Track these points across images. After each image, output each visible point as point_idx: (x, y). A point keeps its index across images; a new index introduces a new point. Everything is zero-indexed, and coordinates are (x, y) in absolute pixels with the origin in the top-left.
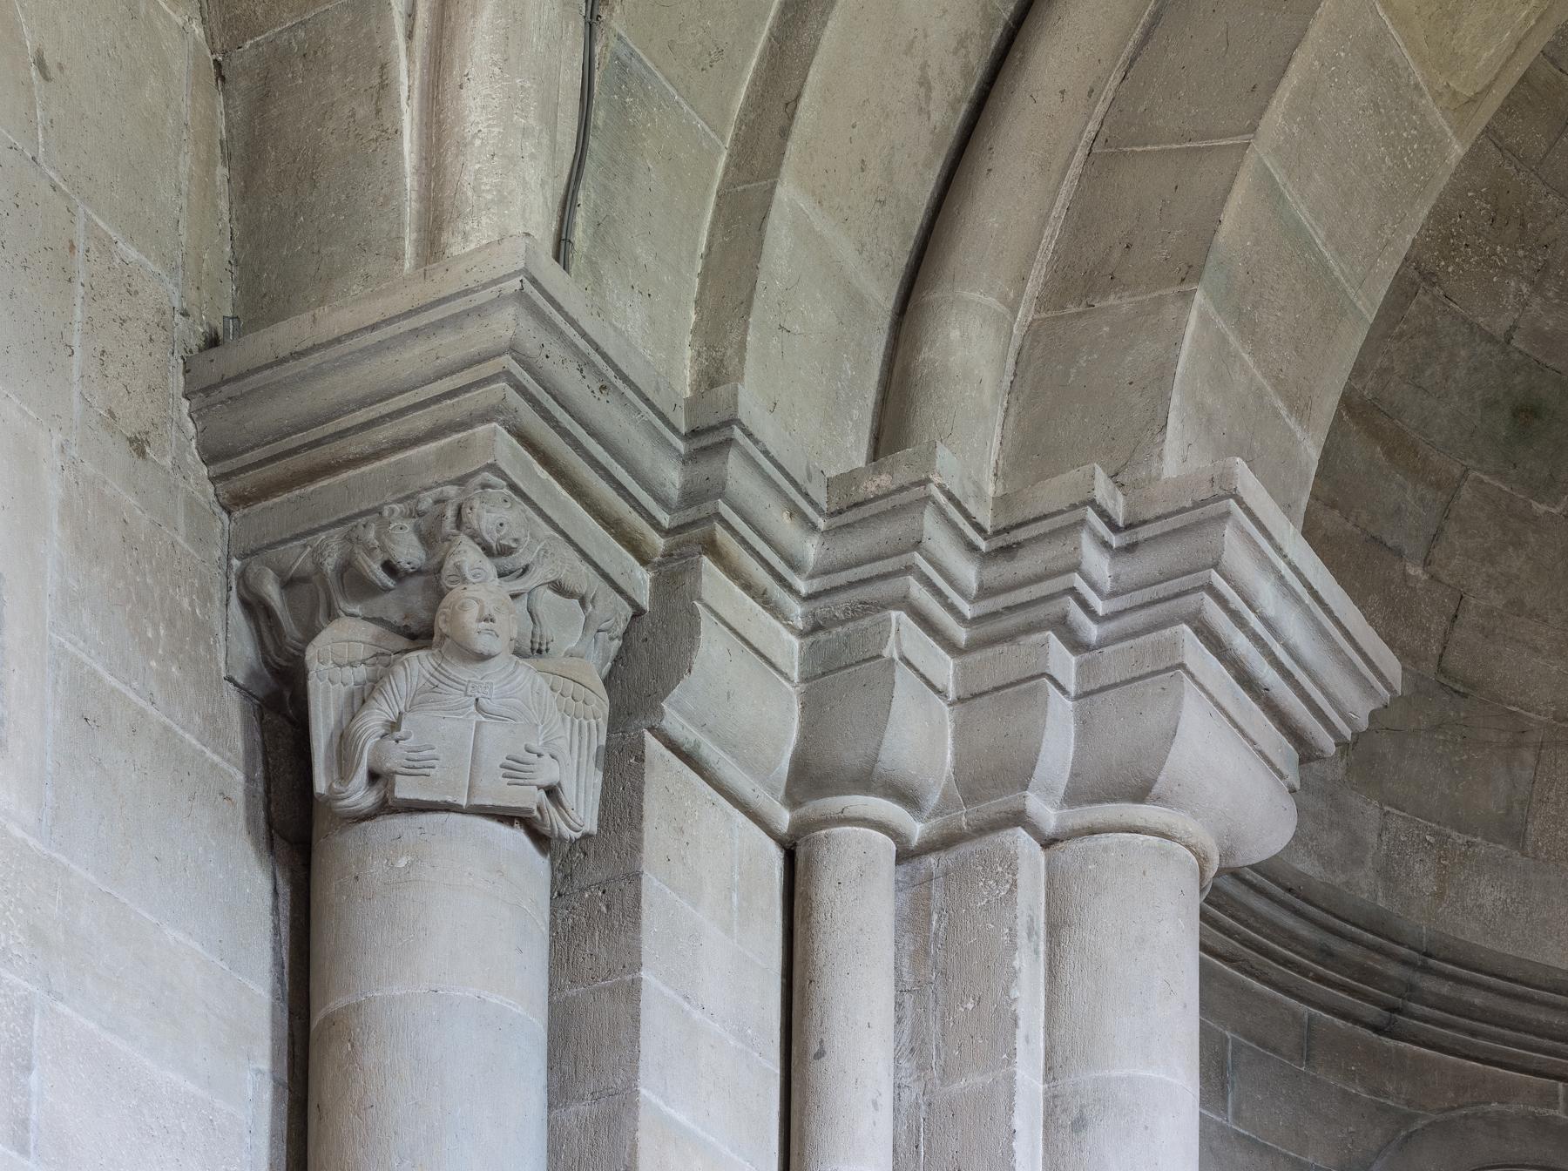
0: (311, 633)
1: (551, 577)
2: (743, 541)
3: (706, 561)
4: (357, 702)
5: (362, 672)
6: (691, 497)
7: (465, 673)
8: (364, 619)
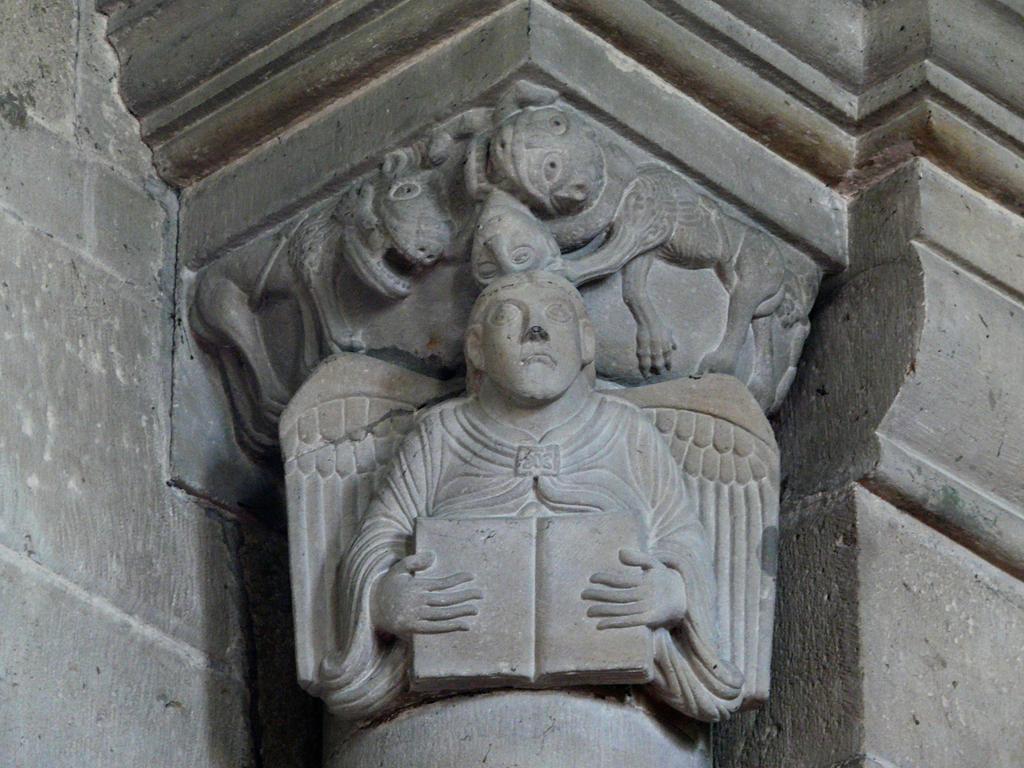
0: (294, 381)
1: (654, 239)
2: (981, 123)
3: (926, 166)
4: (361, 501)
5: (369, 446)
6: (883, 62)
7: (509, 432)
8: (371, 352)
